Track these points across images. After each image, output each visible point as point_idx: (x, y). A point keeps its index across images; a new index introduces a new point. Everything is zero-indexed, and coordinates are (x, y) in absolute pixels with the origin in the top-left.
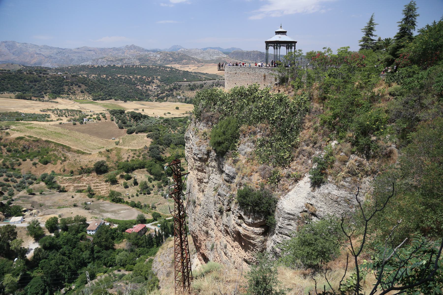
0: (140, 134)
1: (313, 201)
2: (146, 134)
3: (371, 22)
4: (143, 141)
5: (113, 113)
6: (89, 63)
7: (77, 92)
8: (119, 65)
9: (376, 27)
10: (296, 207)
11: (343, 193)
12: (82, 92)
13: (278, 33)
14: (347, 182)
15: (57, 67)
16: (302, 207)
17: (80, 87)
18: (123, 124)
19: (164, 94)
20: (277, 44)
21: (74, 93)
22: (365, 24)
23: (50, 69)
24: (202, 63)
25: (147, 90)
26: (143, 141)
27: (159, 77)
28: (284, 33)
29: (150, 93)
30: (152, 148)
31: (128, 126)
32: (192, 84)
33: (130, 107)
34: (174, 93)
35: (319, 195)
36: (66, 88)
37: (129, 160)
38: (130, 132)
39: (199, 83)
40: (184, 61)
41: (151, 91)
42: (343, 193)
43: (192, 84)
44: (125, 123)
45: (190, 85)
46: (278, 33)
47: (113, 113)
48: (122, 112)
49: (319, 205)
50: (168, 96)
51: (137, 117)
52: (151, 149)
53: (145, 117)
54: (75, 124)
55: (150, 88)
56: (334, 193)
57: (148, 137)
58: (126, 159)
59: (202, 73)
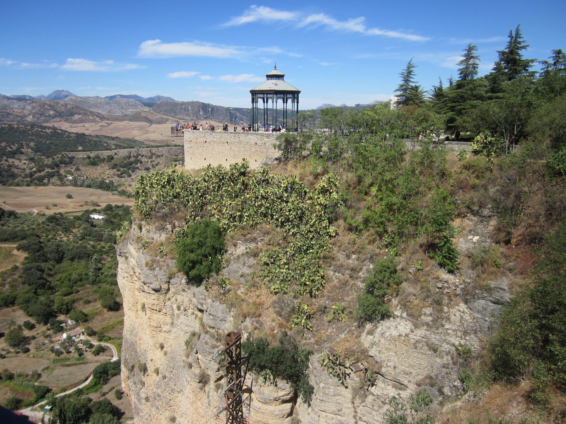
13: (269, 77)
19: (43, 174)
20: (266, 94)
22: (439, 81)
24: (108, 120)
25: (10, 166)
27: (32, 144)
28: (280, 77)
29: (16, 171)
35: (383, 341)
39: (105, 154)
40: (77, 117)
45: (89, 157)
46: (269, 77)
55: (17, 163)
59: (109, 137)
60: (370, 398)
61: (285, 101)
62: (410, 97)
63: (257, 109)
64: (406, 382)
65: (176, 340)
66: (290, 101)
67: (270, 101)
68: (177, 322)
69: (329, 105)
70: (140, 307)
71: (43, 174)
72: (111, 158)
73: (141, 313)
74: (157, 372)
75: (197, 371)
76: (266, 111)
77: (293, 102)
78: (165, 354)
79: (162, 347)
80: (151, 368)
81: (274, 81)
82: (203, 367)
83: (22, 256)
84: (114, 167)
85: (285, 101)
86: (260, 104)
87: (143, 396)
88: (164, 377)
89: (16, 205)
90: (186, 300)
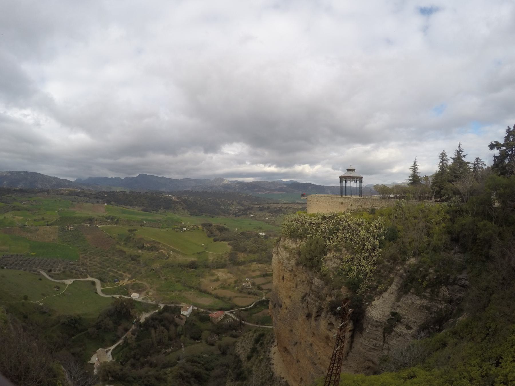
0: (223, 242)
1: (398, 310)
2: (227, 243)
3: (415, 164)
4: (226, 247)
5: (204, 225)
6: (189, 189)
7: (180, 209)
8: (210, 191)
9: (419, 167)
10: (383, 316)
11: (425, 302)
12: (183, 209)
14: (427, 293)
15: (168, 191)
16: (389, 316)
17: (182, 205)
18: (211, 234)
19: (240, 213)
21: (177, 209)
23: (164, 192)
25: (228, 209)
26: (226, 247)
27: (237, 201)
29: (230, 212)
30: (232, 254)
31: (214, 236)
32: (261, 206)
33: (218, 221)
34: (248, 213)
35: (403, 305)
36: (173, 206)
37: (214, 261)
38: (215, 240)
39: (267, 206)
40: (256, 189)
41: (231, 210)
42: (425, 302)
43: (261, 206)
44: (212, 233)
45: (259, 207)
47: (204, 225)
48: (210, 225)
49: (404, 313)
50: (243, 214)
51: (221, 229)
52: (231, 254)
53: (227, 230)
54: (177, 232)
55: (231, 208)
56: (417, 302)
57: (229, 244)
58: (211, 261)
60: (393, 333)
61: (356, 182)
62: (415, 179)
63: (342, 187)
64: (412, 326)
65: (297, 296)
66: (358, 182)
67: (349, 182)
68: (298, 287)
69: (394, 183)
70: (281, 278)
71: (240, 213)
72: (269, 208)
73: (282, 281)
74: (287, 308)
75: (306, 312)
76: (346, 187)
77: (360, 182)
78: (291, 301)
79: (290, 297)
80: (284, 306)
81: (350, 172)
82: (309, 309)
83: (230, 247)
84: (270, 212)
85: (356, 182)
86: (344, 184)
87: (279, 318)
88: (290, 311)
89: (247, 297)
90: (304, 277)
